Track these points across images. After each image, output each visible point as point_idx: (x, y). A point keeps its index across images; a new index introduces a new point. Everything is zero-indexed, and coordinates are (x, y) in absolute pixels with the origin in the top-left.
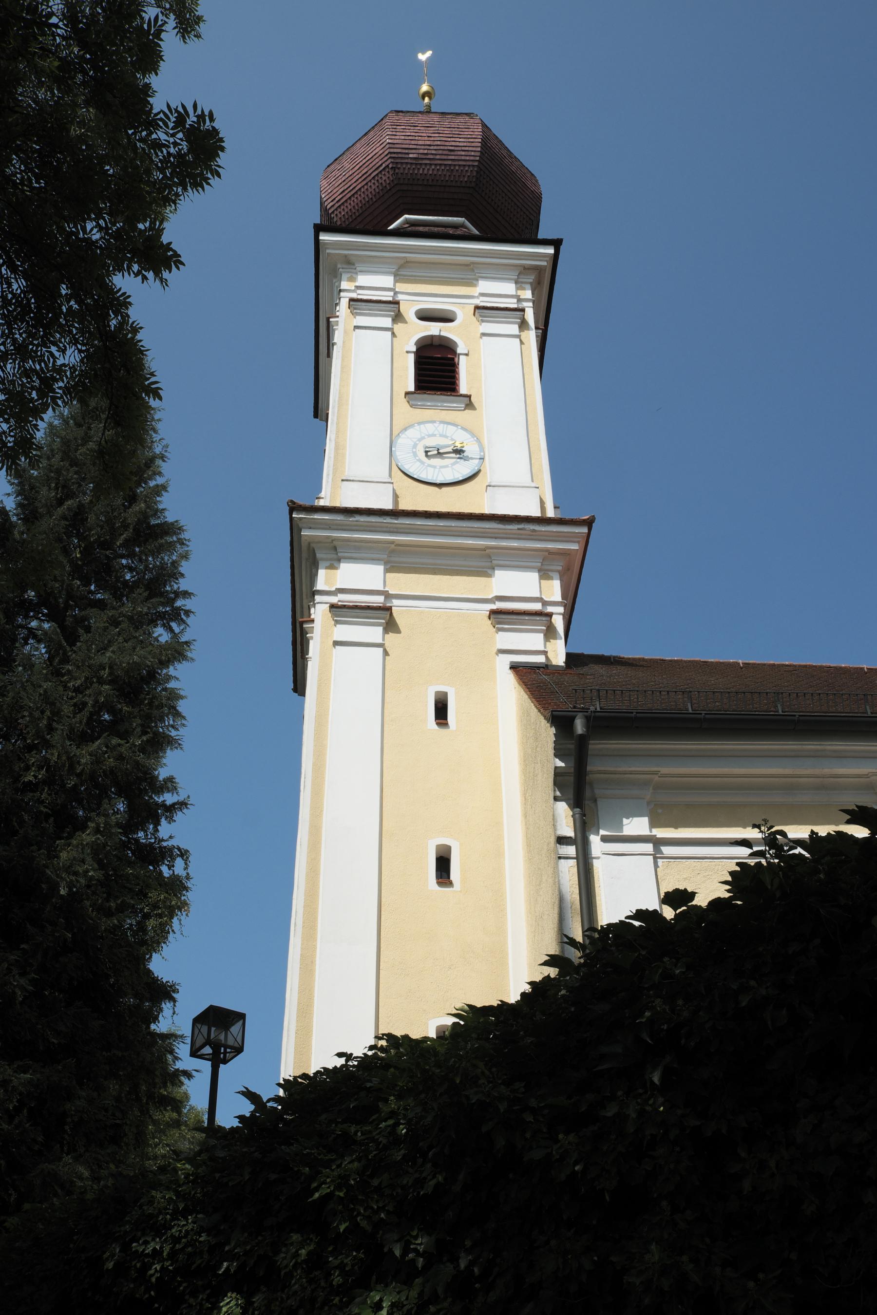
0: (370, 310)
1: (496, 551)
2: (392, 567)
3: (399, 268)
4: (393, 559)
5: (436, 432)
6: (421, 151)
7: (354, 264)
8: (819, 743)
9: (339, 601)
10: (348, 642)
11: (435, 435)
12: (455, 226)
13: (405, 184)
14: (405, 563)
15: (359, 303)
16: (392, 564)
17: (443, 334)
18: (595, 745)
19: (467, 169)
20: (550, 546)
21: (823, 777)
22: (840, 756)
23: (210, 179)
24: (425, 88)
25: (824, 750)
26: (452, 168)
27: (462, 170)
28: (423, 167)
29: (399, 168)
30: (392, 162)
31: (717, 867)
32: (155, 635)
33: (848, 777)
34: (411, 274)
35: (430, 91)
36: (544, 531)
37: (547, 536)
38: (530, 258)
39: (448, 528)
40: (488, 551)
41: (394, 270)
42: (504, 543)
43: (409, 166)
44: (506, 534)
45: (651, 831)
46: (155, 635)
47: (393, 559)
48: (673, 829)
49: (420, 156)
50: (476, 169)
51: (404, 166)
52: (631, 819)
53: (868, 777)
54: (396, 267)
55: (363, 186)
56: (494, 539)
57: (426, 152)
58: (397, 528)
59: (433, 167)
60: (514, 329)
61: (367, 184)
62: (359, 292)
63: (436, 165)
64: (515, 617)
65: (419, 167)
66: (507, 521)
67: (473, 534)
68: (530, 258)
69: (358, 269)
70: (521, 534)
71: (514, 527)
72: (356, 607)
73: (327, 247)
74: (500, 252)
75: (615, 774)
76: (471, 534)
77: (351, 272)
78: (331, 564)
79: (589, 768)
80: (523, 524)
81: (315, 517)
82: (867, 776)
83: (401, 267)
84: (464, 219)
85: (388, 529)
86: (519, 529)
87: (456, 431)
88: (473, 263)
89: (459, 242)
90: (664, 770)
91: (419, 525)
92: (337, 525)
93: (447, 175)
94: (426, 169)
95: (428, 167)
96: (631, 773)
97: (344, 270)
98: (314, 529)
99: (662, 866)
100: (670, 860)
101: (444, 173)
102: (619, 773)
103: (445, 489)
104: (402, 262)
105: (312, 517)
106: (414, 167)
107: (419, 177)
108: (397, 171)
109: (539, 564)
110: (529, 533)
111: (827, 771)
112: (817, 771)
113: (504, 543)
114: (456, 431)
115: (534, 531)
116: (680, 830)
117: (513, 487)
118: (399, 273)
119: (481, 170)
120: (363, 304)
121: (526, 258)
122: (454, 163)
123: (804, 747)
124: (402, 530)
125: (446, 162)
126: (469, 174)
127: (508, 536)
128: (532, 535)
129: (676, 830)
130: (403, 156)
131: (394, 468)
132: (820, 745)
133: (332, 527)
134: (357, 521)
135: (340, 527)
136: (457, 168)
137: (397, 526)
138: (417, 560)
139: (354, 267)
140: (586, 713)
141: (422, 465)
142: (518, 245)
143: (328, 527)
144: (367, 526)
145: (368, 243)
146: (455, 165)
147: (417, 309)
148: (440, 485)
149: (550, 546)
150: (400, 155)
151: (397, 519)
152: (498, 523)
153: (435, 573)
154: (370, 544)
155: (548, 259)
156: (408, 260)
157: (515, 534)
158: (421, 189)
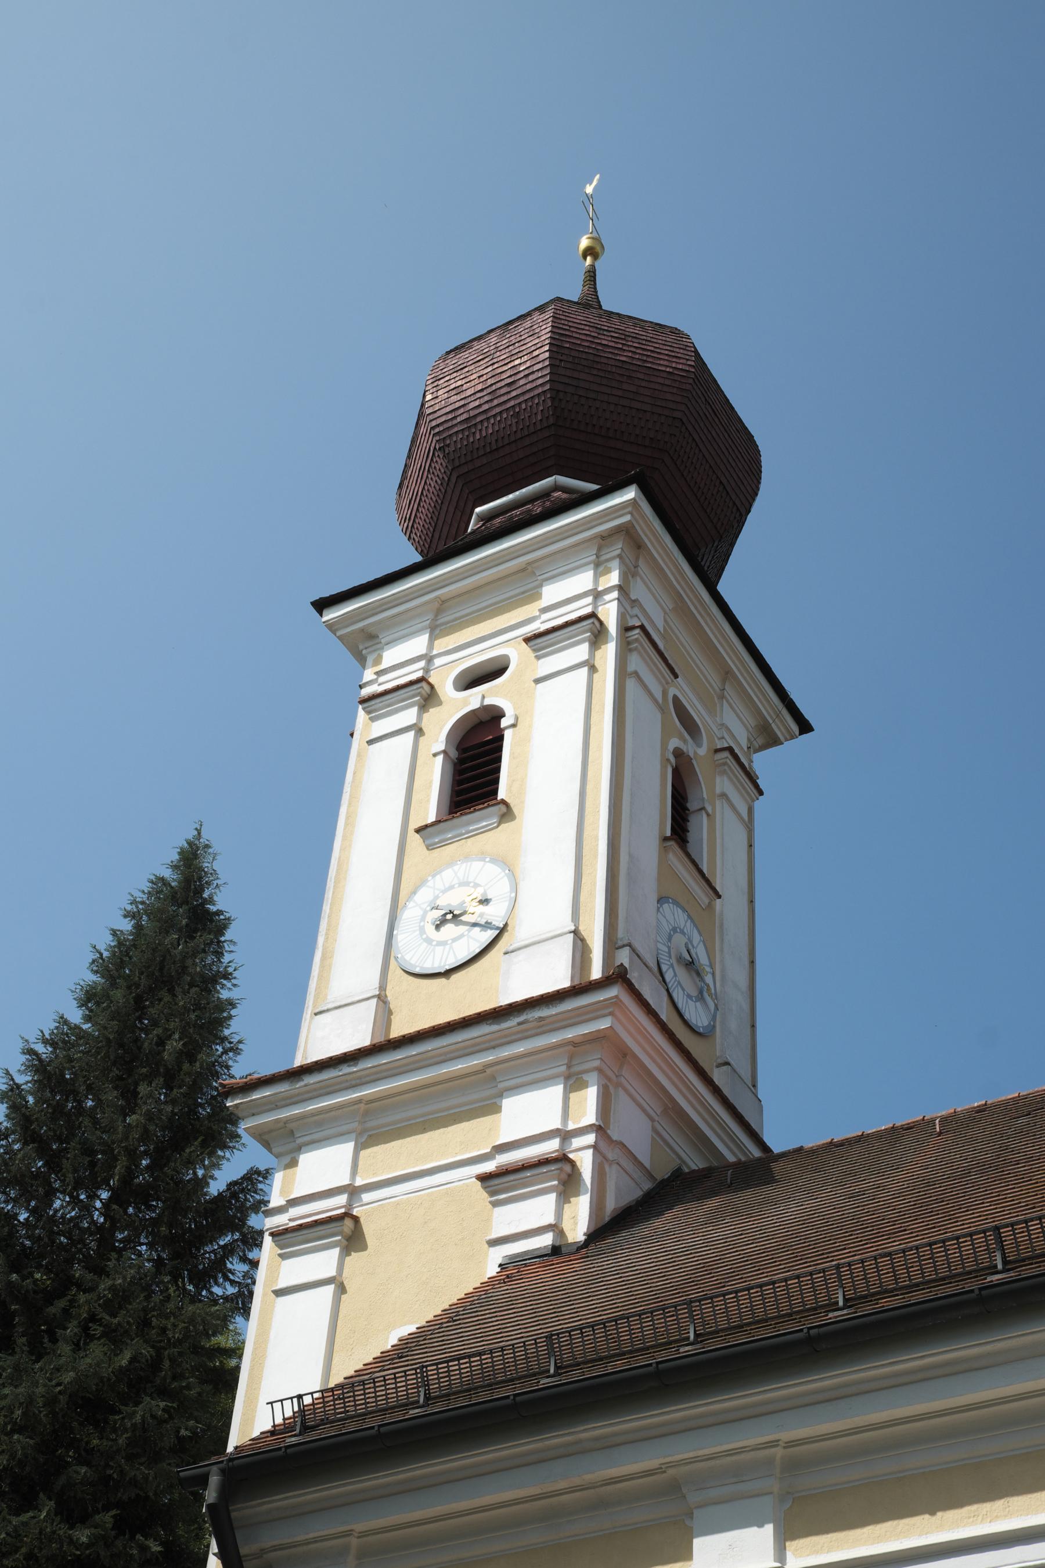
0: (389, 706)
1: (498, 1067)
3: (436, 616)
4: (369, 1124)
5: (437, 892)
6: (472, 405)
7: (378, 637)
8: (567, 1432)
9: (290, 1220)
10: (290, 1287)
11: (452, 887)
12: (545, 494)
13: (464, 464)
14: (383, 1126)
15: (373, 702)
16: (370, 1133)
17: (487, 702)
18: (242, 1511)
19: (536, 401)
20: (570, 1034)
21: (594, 1488)
22: (607, 1445)
24: (584, 243)
25: (580, 1441)
26: (517, 410)
27: (531, 407)
28: (479, 427)
29: (448, 446)
30: (437, 441)
33: (633, 1479)
34: (453, 617)
35: (594, 245)
36: (556, 1014)
37: (563, 1020)
38: (603, 520)
39: (424, 1056)
40: (489, 1071)
41: (428, 622)
42: (506, 1052)
43: (460, 436)
44: (506, 1036)
47: (369, 1124)
49: (472, 413)
50: (549, 396)
51: (454, 439)
53: (665, 1472)
54: (431, 616)
55: (424, 487)
56: (491, 1051)
57: (477, 403)
58: (360, 1078)
59: (492, 421)
60: (581, 652)
61: (425, 482)
62: (382, 679)
63: (494, 416)
64: (512, 1177)
65: (473, 430)
66: (503, 1015)
67: (461, 1053)
68: (603, 520)
69: (383, 641)
70: (526, 1030)
71: (512, 1022)
72: (317, 1223)
73: (336, 627)
74: (559, 531)
75: (295, 1546)
76: (457, 1054)
77: (375, 651)
78: (292, 1158)
79: (243, 1551)
80: (525, 1014)
81: (254, 1097)
83: (438, 612)
84: (554, 477)
85: (348, 1084)
86: (519, 1024)
87: (483, 866)
88: (529, 564)
89: (503, 540)
91: (385, 1064)
92: (284, 1099)
93: (514, 424)
94: (484, 428)
95: (486, 424)
96: (315, 1541)
97: (368, 650)
98: (258, 1114)
101: (509, 422)
102: (299, 1545)
103: (455, 977)
104: (436, 605)
105: (249, 1099)
106: (467, 433)
107: (476, 446)
108: (561, 395)
109: (563, 1068)
110: (535, 1024)
113: (506, 1052)
114: (483, 866)
115: (541, 1019)
117: (539, 942)
118: (439, 622)
119: (558, 391)
120: (378, 700)
121: (600, 521)
122: (517, 401)
123: (547, 1443)
124: (368, 1079)
125: (536, 392)
126: (541, 408)
127: (509, 1039)
128: (543, 1026)
130: (450, 424)
131: (393, 964)
133: (278, 1104)
134: (306, 1085)
135: (288, 1101)
136: (523, 406)
137: (359, 1074)
138: (398, 1117)
139: (377, 641)
140: (221, 1465)
141: (429, 946)
142: (584, 507)
143: (273, 1106)
144: (321, 1088)
145: (394, 594)
146: (520, 403)
147: (453, 679)
148: (448, 973)
149: (570, 1034)
150: (446, 426)
151: (355, 1065)
152: (490, 1024)
153: (424, 1130)
154: (333, 1113)
155: (630, 509)
156: (443, 598)
157: (518, 1032)
158: (485, 462)
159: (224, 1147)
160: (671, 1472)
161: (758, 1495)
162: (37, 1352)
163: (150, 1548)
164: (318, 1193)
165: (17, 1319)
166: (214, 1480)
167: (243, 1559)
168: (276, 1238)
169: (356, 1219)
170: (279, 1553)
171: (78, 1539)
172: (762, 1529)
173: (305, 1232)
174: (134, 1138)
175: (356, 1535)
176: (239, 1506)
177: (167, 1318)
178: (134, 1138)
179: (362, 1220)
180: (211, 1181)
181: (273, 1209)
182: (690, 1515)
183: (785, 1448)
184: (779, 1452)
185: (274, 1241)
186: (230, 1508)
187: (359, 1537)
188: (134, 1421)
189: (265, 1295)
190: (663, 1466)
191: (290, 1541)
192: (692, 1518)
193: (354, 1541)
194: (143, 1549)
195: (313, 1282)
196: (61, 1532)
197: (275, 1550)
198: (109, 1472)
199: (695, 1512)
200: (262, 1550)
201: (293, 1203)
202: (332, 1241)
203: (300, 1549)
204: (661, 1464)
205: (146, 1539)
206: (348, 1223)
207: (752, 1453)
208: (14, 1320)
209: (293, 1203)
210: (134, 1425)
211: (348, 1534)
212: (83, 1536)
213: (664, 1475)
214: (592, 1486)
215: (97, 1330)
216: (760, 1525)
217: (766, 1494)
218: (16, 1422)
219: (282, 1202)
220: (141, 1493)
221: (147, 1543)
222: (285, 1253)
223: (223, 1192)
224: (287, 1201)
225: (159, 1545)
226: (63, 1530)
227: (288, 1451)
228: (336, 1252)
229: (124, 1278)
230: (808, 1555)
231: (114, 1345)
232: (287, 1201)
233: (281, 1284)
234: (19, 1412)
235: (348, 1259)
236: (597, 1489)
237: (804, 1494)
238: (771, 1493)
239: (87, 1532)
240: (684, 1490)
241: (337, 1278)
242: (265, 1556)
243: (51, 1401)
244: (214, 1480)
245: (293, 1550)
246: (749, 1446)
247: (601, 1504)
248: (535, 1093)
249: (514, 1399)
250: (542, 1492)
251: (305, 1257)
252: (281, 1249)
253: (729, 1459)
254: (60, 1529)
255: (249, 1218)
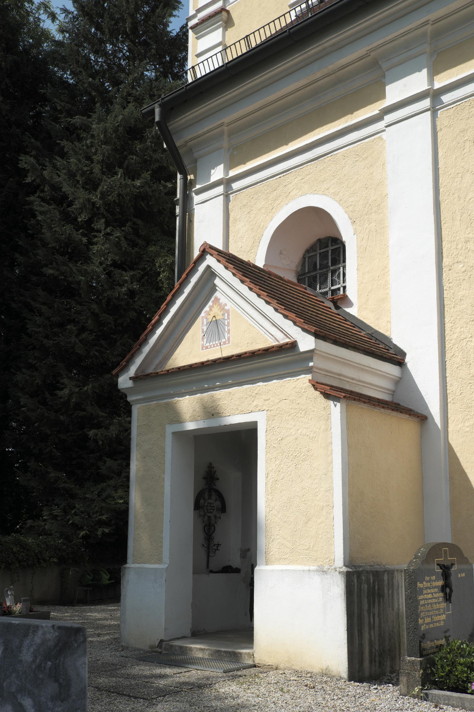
2: (201, 393)
8: (317, 45)
21: (334, 73)
23: (71, 121)
25: (325, 49)
31: (264, 188)
32: (20, 158)
45: (227, 174)
46: (20, 158)
48: (285, 146)
52: (216, 168)
53: (370, 55)
75: (199, 137)
79: (178, 144)
82: (367, 55)
90: (227, 120)
96: (208, 132)
99: (232, 200)
100: (236, 193)
111: (331, 67)
112: (325, 71)
116: (290, 144)
123: (309, 53)
129: (245, 165)
132: (319, 45)
140: (159, 103)
159: (175, 9)
160: (373, 54)
161: (418, 56)
162: (108, 112)
163: (168, 186)
164: (209, 3)
165: (96, 99)
166: (157, 111)
167: (178, 149)
168: (193, 30)
169: (228, 12)
170: (193, 141)
171: (136, 185)
172: (421, 73)
173: (205, 23)
174: (131, 8)
175: (226, 125)
176: (171, 123)
177: (161, 90)
178: (131, 8)
179: (231, 12)
180: (170, 24)
181: (191, 17)
182: (384, 76)
183: (432, 24)
184: (429, 28)
185: (193, 32)
186: (168, 125)
187: (227, 126)
188: (152, 134)
189: (193, 59)
190: (368, 52)
191: (197, 134)
192: (385, 78)
193: (225, 128)
194: (165, 187)
195: (212, 46)
196: (129, 183)
197: (191, 141)
198: (146, 157)
199: (386, 73)
200: (186, 142)
201: (199, 11)
202: (218, 25)
203: (202, 138)
204: (367, 51)
205: (165, 183)
206: (224, 13)
207: (415, 32)
208: (95, 100)
209: (199, 11)
210: (152, 136)
211: (222, 125)
212: (138, 183)
213: (370, 57)
214: (334, 72)
215: (131, 99)
216: (420, 70)
217: (424, 53)
218: (102, 141)
219: (194, 12)
220: (161, 165)
221: (166, 184)
222: (198, 36)
223: (179, 32)
224: (196, 11)
225: (171, 184)
226: (129, 182)
227: (187, 88)
228: (221, 30)
229: (138, 73)
230: (446, 80)
231: (139, 104)
232: (196, 11)
233: (199, 51)
234: (102, 136)
235: (227, 32)
236: (336, 74)
237: (442, 50)
238: (425, 53)
239: (139, 181)
240: (380, 63)
241: (223, 42)
242: (187, 144)
243: (116, 130)
244: (157, 111)
245: (199, 139)
246: (413, 28)
247: (339, 81)
248: (436, 302)
249: (289, 32)
250: (310, 81)
251: (208, 36)
252: (196, 35)
253: (403, 39)
254: (128, 182)
255: (175, 13)
